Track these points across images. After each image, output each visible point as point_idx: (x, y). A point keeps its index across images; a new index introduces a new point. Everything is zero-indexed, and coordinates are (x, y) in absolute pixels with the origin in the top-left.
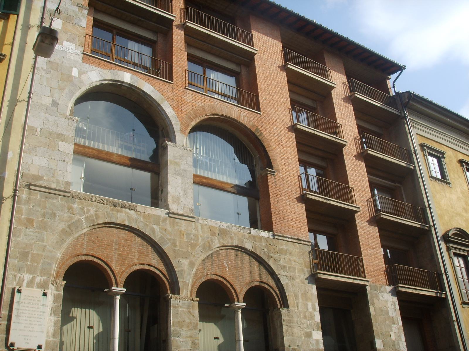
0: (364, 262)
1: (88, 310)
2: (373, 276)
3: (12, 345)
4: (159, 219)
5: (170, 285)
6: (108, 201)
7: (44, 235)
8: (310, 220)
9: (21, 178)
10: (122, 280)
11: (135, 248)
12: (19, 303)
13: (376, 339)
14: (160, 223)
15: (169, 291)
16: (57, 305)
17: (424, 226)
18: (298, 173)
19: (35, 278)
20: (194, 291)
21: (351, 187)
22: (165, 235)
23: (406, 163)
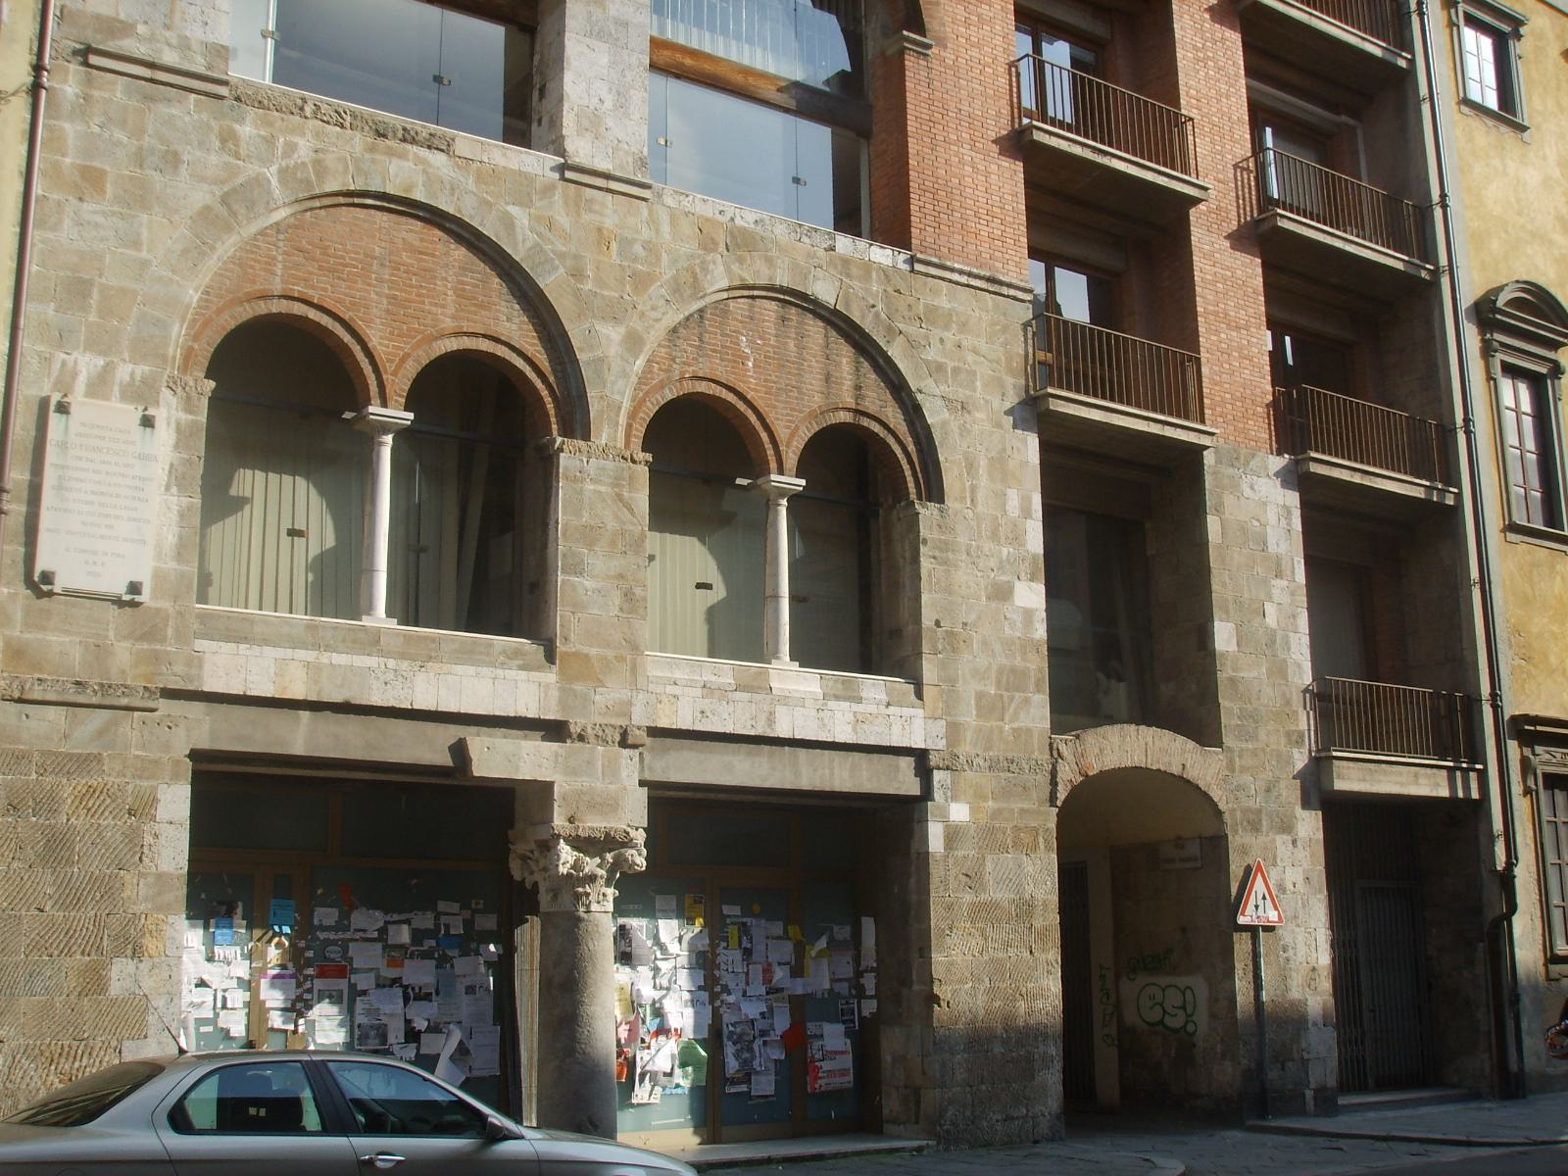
0: (1205, 370)
1: (287, 479)
2: (1230, 417)
3: (47, 578)
4: (527, 186)
5: (557, 407)
6: (359, 118)
7: (141, 225)
8: (1036, 216)
9: (56, 26)
10: (400, 383)
11: (446, 279)
12: (63, 446)
13: (1215, 619)
14: (532, 201)
15: (554, 427)
16: (186, 457)
17: (1419, 266)
18: (1008, 55)
19: (115, 368)
20: (637, 429)
21: (1185, 116)
22: (549, 239)
23: (1384, 45)
